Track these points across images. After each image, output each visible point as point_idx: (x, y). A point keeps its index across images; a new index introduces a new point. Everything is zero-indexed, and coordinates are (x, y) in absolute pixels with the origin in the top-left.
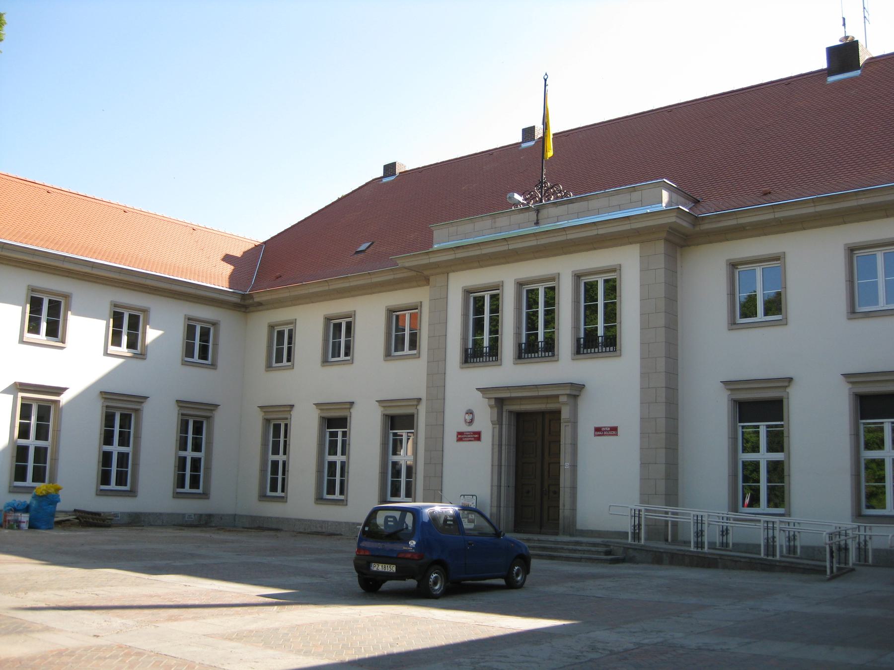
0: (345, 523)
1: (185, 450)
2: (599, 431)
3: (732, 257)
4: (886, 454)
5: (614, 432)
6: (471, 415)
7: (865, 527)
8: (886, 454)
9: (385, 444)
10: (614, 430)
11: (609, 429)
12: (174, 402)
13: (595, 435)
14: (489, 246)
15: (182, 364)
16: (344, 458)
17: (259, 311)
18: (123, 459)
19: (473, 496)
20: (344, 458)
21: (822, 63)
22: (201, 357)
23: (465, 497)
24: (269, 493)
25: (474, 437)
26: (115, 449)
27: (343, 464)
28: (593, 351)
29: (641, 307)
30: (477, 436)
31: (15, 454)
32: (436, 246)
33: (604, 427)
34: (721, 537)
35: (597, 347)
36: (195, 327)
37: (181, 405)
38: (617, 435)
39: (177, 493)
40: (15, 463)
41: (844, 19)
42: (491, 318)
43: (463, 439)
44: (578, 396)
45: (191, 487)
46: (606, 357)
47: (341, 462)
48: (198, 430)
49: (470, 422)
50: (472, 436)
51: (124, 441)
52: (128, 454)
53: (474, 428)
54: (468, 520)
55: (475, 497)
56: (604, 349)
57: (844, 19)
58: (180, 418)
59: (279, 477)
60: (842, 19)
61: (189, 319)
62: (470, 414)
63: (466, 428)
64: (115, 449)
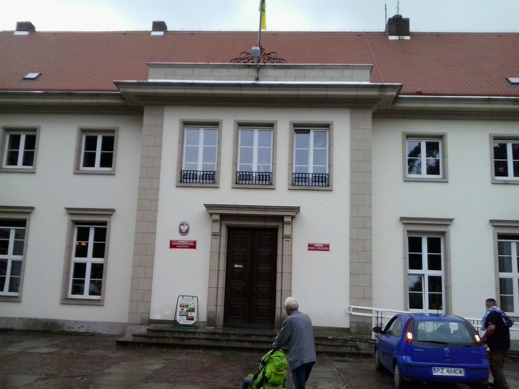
0: (19, 318)
2: (312, 247)
3: (406, 131)
4: (513, 275)
5: (326, 248)
6: (186, 226)
7: (478, 321)
8: (513, 275)
10: (326, 248)
11: (322, 246)
13: (309, 250)
14: (248, 89)
19: (193, 297)
21: (382, 27)
24: (70, 296)
25: (189, 245)
30: (193, 246)
31: (106, 250)
32: (150, 81)
33: (180, 240)
38: (328, 250)
41: (386, 5)
42: (95, 149)
44: (31, 212)
49: (185, 232)
50: (187, 244)
53: (189, 238)
54: (187, 317)
55: (195, 298)
57: (386, 5)
60: (385, 6)
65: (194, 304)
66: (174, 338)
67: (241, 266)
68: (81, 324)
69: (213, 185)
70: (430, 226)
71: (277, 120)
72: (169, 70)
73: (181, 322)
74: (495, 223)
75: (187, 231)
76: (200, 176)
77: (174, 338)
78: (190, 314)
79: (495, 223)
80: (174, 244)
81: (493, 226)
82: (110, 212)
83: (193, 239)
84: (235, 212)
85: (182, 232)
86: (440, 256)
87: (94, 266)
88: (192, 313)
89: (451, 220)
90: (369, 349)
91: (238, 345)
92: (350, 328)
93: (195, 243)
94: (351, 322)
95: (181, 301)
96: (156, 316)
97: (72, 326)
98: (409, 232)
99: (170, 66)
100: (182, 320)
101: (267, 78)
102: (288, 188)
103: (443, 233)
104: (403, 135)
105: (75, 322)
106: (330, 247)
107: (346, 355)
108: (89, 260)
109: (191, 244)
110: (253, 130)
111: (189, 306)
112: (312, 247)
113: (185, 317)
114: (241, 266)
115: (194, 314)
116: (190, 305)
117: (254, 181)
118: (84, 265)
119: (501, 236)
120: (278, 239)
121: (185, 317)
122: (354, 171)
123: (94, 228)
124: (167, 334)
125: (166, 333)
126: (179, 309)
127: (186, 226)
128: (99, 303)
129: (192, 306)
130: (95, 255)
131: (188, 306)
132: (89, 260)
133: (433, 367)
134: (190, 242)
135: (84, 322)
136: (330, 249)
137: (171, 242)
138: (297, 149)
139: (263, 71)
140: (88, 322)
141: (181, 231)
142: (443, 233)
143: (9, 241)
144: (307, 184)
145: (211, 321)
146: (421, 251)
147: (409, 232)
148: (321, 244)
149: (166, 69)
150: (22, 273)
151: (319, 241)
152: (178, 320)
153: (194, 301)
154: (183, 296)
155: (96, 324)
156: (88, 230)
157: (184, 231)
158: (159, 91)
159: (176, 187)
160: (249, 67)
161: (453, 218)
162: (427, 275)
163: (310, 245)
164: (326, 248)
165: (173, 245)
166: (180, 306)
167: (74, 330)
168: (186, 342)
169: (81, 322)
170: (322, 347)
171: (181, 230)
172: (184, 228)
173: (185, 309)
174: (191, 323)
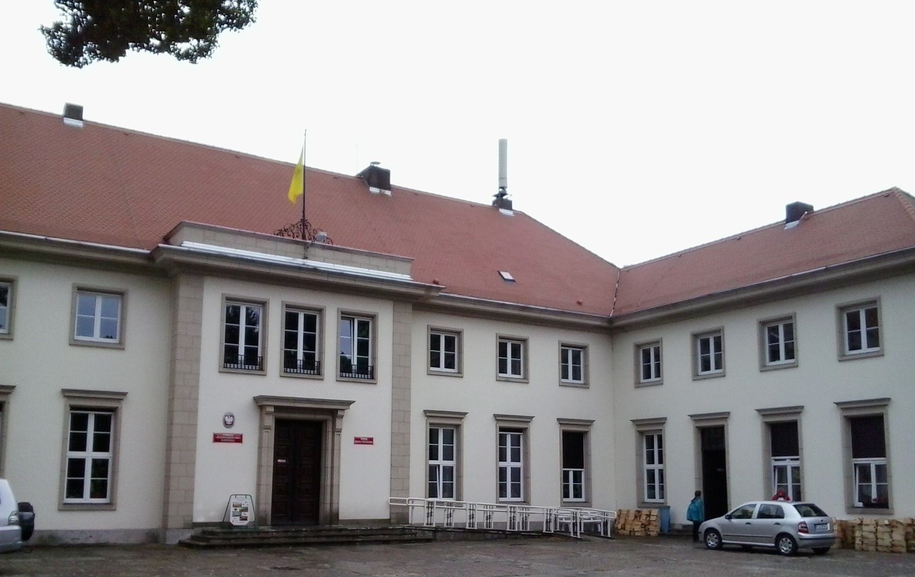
1: (653, 463)
2: (358, 441)
5: (371, 442)
6: (232, 417)
9: (526, 453)
10: (370, 441)
11: (367, 439)
12: (556, 420)
13: (355, 443)
15: (559, 385)
16: (661, 466)
17: (338, 314)
18: (516, 472)
19: (246, 495)
20: (661, 466)
22: (447, 366)
23: (237, 496)
26: (509, 464)
27: (661, 472)
28: (232, 366)
29: (200, 331)
30: (238, 439)
34: (432, 511)
35: (314, 370)
36: (439, 337)
37: (67, 394)
38: (372, 444)
39: (564, 502)
40: (499, 482)
43: (222, 440)
45: (513, 496)
46: (297, 378)
47: (659, 470)
48: (449, 438)
49: (231, 424)
50: (233, 438)
51: (448, 456)
52: (452, 468)
56: (357, 375)
58: (429, 428)
59: (441, 482)
61: (500, 338)
62: (231, 416)
63: (222, 430)
64: (509, 464)
65: (246, 504)
66: (253, 538)
67: (284, 461)
68: (89, 534)
69: (260, 372)
70: (446, 419)
71: (268, 298)
72: (208, 233)
73: (234, 524)
74: (498, 418)
75: (232, 424)
76: (300, 366)
77: (253, 538)
78: (243, 514)
79: (498, 418)
80: (218, 437)
81: (65, 396)
82: (120, 396)
83: (240, 432)
84: (292, 405)
85: (227, 424)
86: (108, 436)
87: (95, 462)
88: (245, 513)
89: (125, 394)
90: (422, 535)
91: (316, 540)
92: (390, 519)
93: (241, 436)
94: (391, 514)
95: (234, 500)
96: (199, 518)
97: (77, 536)
98: (73, 408)
99: (210, 229)
100: (236, 521)
101: (315, 258)
102: (218, 371)
103: (114, 410)
104: (73, 288)
105: (81, 532)
106: (374, 440)
107: (412, 542)
108: (89, 455)
109: (237, 438)
110: (121, 294)
111: (242, 506)
112: (358, 441)
113: (238, 518)
114: (284, 461)
115: (247, 514)
116: (243, 504)
117: (299, 369)
118: (82, 462)
119: (501, 429)
120: (800, 450)
121: (238, 518)
122: (396, 365)
123: (94, 415)
124: (249, 536)
125: (239, 534)
126: (232, 509)
127: (232, 417)
128: (110, 506)
129: (245, 506)
130: (96, 449)
131: (241, 506)
132: (89, 455)
133: (829, 529)
134: (235, 435)
135: (94, 531)
136: (374, 443)
137: (215, 435)
138: (252, 327)
139: (312, 250)
140: (98, 531)
141: (226, 424)
142: (114, 410)
143: (86, 433)
144: (239, 367)
145: (260, 520)
146: (86, 429)
147: (73, 408)
148: (366, 438)
149: (353, 256)
150: (888, 479)
151: (364, 435)
152: (231, 521)
153: (247, 500)
154: (236, 495)
155: (108, 533)
156: (85, 417)
157: (229, 424)
158: (331, 280)
159: (219, 373)
160: (297, 243)
161: (127, 392)
162: (91, 458)
163: (356, 439)
164: (370, 441)
165: (217, 439)
166: (233, 506)
167: (79, 542)
168: (266, 541)
169: (90, 531)
170: (442, 534)
171: (225, 422)
172: (229, 420)
173: (238, 509)
174: (245, 523)
